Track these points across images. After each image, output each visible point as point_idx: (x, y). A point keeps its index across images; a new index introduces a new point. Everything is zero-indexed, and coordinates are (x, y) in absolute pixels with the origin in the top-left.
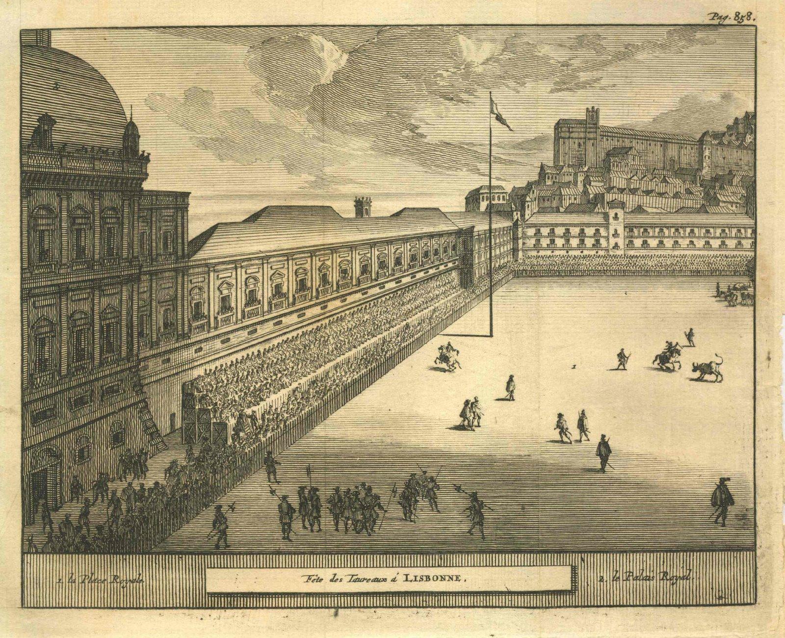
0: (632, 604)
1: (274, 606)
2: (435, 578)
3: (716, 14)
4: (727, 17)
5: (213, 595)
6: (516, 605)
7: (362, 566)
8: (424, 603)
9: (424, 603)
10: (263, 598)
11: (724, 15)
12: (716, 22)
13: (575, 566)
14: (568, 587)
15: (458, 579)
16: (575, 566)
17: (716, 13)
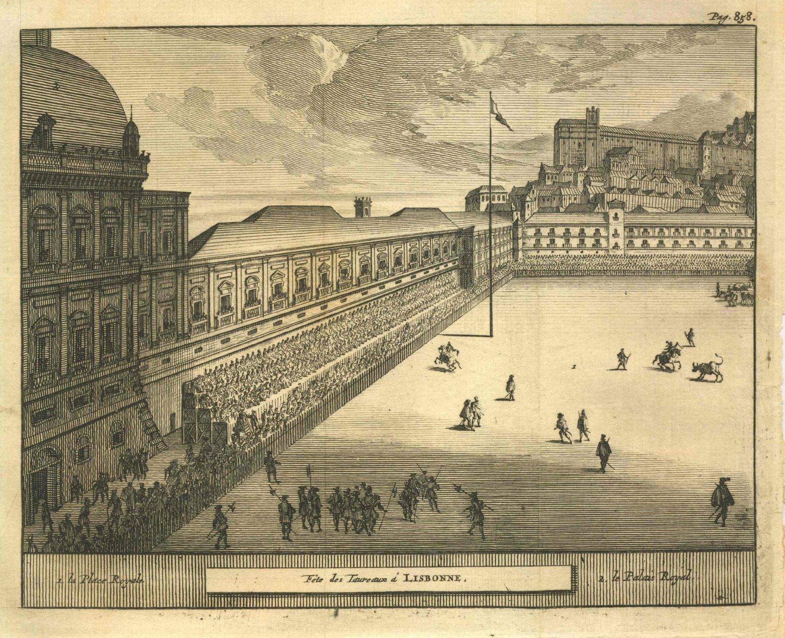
0: (632, 604)
1: (274, 606)
2: (435, 578)
3: (716, 14)
4: (727, 17)
5: (213, 595)
6: (516, 605)
7: (362, 566)
8: (424, 603)
9: (424, 603)
10: (263, 598)
11: (724, 15)
12: (716, 22)
13: (575, 566)
14: (568, 587)
15: (458, 579)
16: (575, 566)
17: (716, 13)
